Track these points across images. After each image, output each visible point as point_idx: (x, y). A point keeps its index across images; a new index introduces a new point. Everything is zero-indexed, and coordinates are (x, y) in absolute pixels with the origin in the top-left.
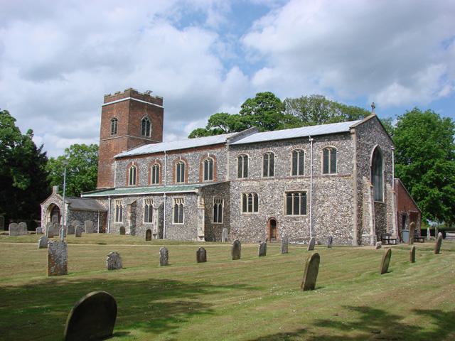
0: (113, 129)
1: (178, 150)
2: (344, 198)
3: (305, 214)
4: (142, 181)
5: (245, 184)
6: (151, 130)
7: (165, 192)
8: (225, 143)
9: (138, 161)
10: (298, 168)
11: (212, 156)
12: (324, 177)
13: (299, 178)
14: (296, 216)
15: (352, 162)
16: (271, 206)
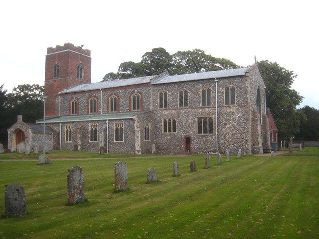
0: (55, 73)
2: (241, 121)
3: (213, 133)
5: (166, 112)
6: (83, 74)
7: (107, 119)
8: (149, 83)
10: (206, 100)
13: (207, 108)
14: (204, 134)
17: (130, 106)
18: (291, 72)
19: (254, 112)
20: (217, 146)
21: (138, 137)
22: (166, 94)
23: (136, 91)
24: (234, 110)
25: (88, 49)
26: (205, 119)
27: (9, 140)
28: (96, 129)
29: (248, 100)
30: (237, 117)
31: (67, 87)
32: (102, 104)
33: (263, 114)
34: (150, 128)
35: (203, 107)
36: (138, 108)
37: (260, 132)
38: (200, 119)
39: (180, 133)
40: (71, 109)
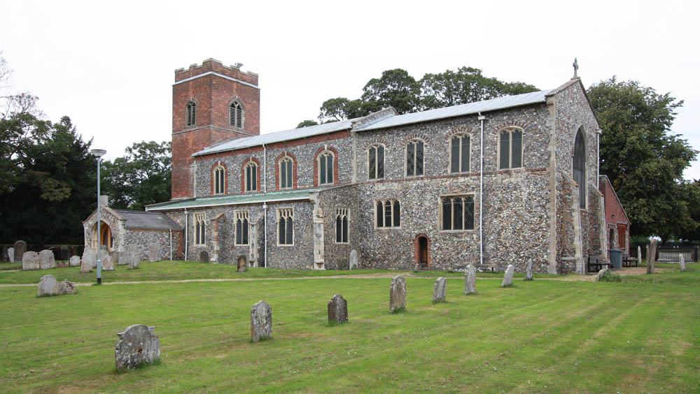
1: (251, 148)
3: (472, 228)
4: (233, 186)
5: (380, 187)
6: (243, 119)
7: (265, 201)
8: (350, 129)
9: (227, 160)
10: (460, 160)
11: (331, 149)
12: (500, 173)
13: (462, 176)
15: (549, 149)
16: (420, 218)
17: (315, 176)
18: (667, 95)
19: (564, 184)
20: (481, 255)
21: (319, 236)
22: (381, 150)
23: (326, 146)
24: (519, 180)
25: (254, 71)
26: (458, 199)
27: (86, 244)
28: (246, 221)
29: (550, 156)
30: (525, 196)
31: (209, 142)
32: (266, 174)
33: (591, 188)
34: (349, 219)
35: (454, 174)
36: (330, 180)
37: (578, 227)
38: (446, 200)
39: (408, 228)
40: (246, 172)
